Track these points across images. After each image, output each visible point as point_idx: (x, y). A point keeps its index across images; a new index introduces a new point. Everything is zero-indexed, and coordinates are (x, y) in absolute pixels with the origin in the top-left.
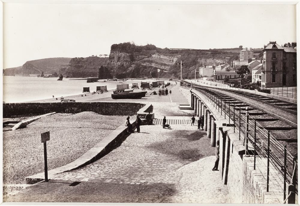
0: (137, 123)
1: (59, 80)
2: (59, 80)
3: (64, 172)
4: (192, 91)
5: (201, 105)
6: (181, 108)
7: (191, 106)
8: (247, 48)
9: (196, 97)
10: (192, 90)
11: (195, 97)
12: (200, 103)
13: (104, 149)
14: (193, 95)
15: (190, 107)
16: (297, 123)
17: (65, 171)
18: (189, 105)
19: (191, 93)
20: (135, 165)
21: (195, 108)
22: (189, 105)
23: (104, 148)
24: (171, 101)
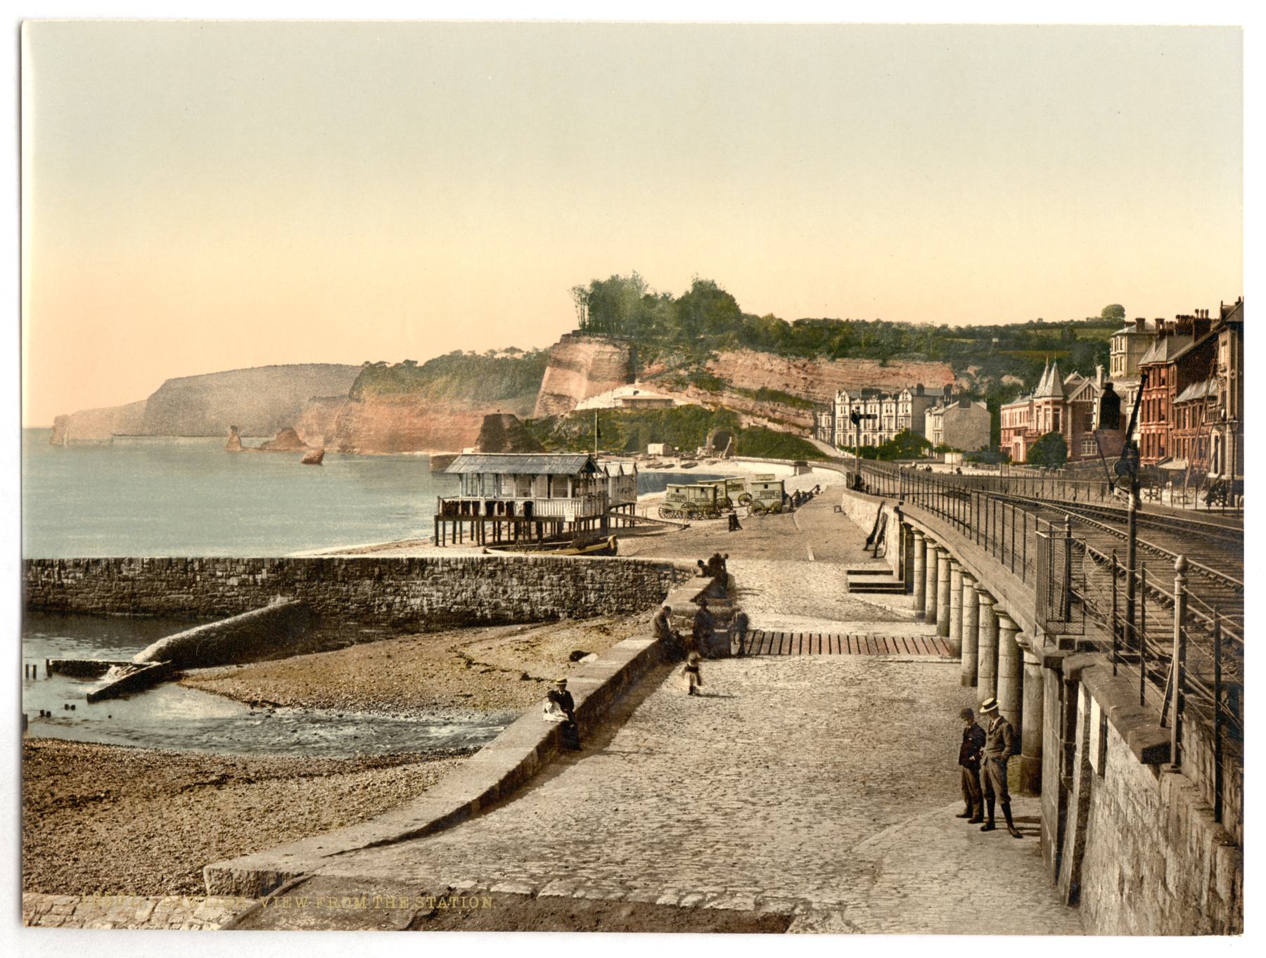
0: (744, 426)
1: (983, 829)
2: (983, 829)
3: (371, 846)
4: (901, 508)
5: (949, 570)
6: (856, 588)
7: (901, 578)
8: (1141, 321)
9: (921, 533)
10: (901, 504)
11: (917, 537)
12: (942, 564)
13: (531, 754)
14: (908, 526)
15: (893, 579)
16: (1243, 626)
17: (374, 841)
18: (890, 573)
19: (901, 519)
20: (672, 827)
21: (916, 587)
22: (890, 573)
23: (531, 749)
24: (811, 557)
